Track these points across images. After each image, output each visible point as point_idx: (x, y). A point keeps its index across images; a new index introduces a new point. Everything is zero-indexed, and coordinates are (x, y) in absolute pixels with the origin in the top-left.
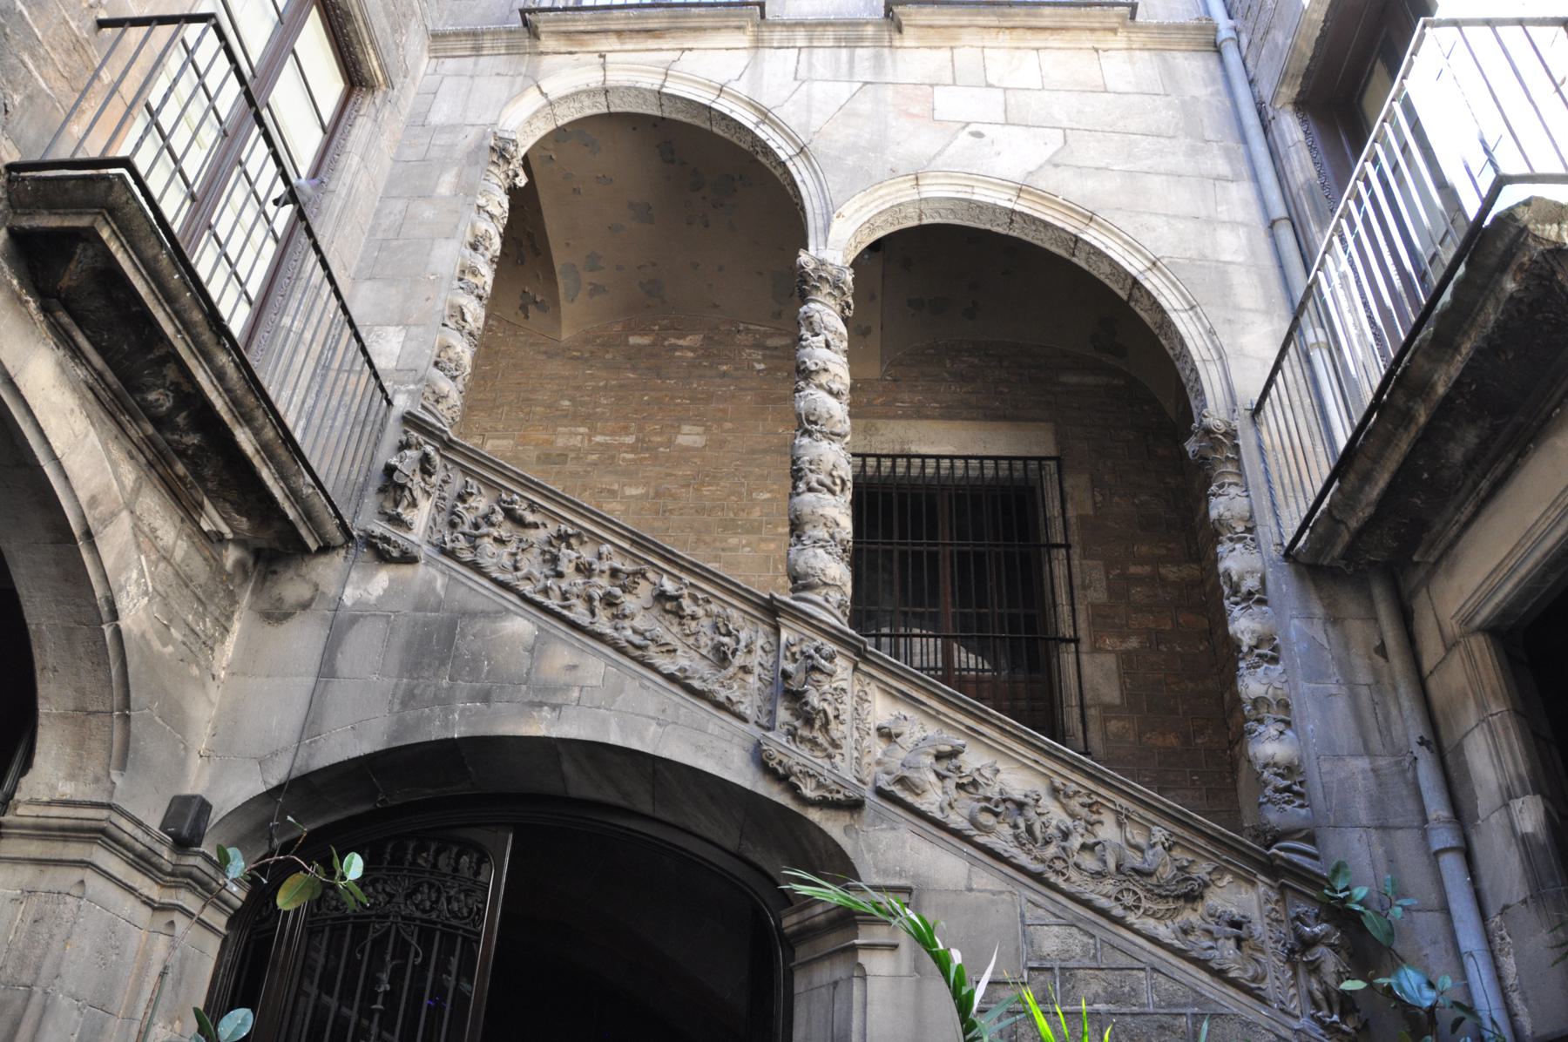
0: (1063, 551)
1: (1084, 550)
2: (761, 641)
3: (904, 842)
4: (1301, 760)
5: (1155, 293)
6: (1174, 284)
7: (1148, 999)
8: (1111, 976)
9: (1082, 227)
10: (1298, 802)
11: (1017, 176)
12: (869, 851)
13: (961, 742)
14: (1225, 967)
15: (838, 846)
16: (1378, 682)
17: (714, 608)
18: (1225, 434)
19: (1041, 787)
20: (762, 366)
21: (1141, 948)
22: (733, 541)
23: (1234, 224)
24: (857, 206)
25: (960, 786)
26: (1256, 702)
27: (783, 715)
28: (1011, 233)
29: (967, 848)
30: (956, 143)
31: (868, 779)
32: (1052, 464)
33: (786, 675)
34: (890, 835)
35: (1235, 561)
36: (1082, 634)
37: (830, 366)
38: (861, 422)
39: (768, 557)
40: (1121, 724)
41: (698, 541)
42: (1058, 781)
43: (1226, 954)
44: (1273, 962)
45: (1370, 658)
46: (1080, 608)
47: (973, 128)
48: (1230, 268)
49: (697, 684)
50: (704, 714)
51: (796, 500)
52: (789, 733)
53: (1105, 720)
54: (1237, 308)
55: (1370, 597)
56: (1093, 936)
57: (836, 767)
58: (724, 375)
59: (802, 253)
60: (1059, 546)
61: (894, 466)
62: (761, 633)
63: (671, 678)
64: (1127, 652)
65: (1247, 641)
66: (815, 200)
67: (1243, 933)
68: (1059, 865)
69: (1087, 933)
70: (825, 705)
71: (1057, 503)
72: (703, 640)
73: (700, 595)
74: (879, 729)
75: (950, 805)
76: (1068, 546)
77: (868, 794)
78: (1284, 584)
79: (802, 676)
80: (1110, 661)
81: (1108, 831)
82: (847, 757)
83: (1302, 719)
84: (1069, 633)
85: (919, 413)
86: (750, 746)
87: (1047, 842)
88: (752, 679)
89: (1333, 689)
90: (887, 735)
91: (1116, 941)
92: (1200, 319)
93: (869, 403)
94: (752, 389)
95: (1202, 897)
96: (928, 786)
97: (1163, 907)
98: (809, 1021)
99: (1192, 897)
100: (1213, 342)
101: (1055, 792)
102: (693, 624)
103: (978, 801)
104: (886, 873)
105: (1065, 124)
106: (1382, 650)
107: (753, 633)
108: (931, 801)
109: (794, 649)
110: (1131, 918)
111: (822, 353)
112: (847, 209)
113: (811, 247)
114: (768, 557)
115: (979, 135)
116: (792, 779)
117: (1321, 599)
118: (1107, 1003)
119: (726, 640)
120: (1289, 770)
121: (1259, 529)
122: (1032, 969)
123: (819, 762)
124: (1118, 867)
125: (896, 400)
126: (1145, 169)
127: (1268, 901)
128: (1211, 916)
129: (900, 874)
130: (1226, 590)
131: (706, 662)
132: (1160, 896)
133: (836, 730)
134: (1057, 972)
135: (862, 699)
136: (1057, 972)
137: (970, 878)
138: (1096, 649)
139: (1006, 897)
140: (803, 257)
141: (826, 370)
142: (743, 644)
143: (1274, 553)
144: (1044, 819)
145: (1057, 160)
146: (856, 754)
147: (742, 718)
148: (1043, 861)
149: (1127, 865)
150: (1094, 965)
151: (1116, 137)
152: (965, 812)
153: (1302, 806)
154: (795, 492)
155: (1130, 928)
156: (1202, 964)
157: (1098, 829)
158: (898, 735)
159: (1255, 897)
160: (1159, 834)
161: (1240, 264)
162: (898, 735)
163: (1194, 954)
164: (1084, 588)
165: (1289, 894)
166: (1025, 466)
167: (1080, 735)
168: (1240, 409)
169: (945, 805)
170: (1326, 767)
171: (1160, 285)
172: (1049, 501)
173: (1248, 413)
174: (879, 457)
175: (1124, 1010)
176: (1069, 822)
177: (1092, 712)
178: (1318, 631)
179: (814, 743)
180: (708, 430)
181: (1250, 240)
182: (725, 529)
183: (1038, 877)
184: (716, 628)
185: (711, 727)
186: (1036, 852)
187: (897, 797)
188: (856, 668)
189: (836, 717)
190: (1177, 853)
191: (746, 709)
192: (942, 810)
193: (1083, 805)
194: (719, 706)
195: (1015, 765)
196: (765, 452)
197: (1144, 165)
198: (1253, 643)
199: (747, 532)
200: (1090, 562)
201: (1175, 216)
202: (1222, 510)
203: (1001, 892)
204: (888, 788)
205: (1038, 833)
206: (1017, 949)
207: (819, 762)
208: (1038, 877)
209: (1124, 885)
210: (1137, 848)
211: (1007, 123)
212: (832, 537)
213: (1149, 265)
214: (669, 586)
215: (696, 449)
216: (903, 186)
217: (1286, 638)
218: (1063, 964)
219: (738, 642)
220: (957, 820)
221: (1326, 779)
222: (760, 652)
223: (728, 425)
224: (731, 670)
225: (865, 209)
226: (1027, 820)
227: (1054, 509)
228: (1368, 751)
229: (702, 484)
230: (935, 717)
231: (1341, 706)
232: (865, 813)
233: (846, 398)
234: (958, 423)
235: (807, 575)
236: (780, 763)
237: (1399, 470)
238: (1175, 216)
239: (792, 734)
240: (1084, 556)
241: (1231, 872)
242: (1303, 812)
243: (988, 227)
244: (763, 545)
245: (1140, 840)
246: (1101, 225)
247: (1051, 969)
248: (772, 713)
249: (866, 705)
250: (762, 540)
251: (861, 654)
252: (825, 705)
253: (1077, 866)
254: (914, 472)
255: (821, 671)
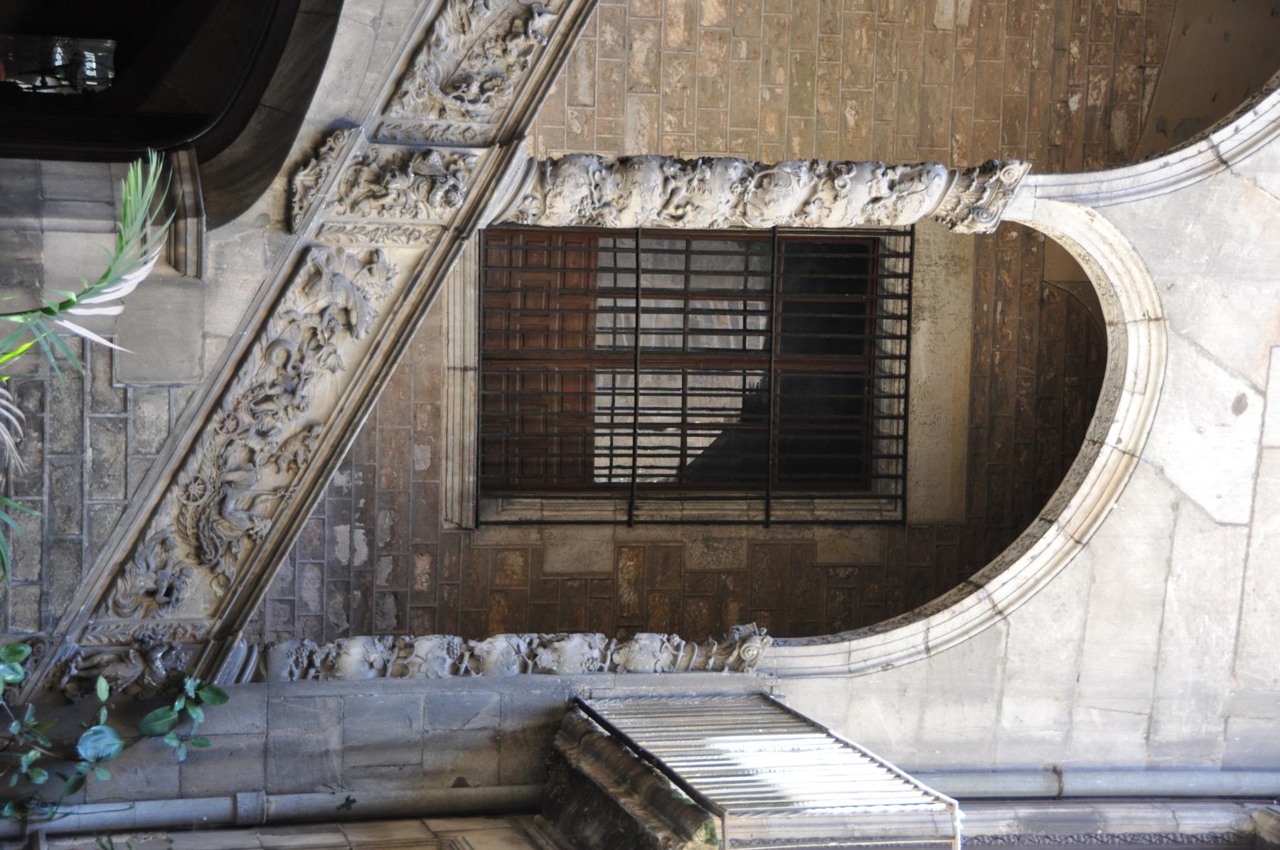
0: (761, 517)
1: (764, 545)
2: (476, 126)
3: (252, 273)
4: (339, 678)
5: (956, 608)
6: (966, 632)
7: (97, 500)
8: (119, 467)
9: (1070, 530)
10: (297, 672)
11: (1158, 451)
12: (243, 238)
13: (363, 335)
14: (127, 576)
15: (247, 207)
16: (425, 774)
17: (517, 75)
18: (740, 660)
19: (314, 412)
20: (1074, 103)
21: (146, 499)
22: (780, 76)
23: (1069, 726)
24: (1111, 238)
25: (314, 332)
26: (410, 647)
27: (388, 152)
28: (1085, 442)
29: (247, 336)
30: (1223, 377)
31: (322, 239)
32: (898, 515)
33: (426, 154)
34: (259, 259)
35: (578, 650)
36: (641, 533)
37: (841, 203)
38: (969, 253)
39: (754, 124)
40: (518, 569)
41: (781, 27)
42: (320, 430)
43: (141, 579)
44: (134, 624)
45: (453, 771)
46: (678, 532)
47: (1254, 400)
48: (990, 709)
49: (422, 58)
50: (387, 68)
51: (655, 164)
52: (365, 158)
53: (523, 550)
54: (924, 705)
55: (525, 784)
56: (158, 452)
57: (328, 206)
58: (1061, 49)
59: (1027, 166)
60: (767, 511)
61: (895, 296)
62: (487, 126)
63: (430, 29)
64: (615, 587)
65: (480, 647)
66: (1128, 182)
67: (161, 597)
68: (230, 424)
69: (161, 446)
70: (393, 196)
71: (834, 516)
72: (478, 64)
73: (530, 58)
74: (377, 251)
75: (293, 321)
76: (766, 523)
77: (307, 236)
78: (541, 694)
79: (426, 171)
80: (603, 563)
81: (268, 478)
82: (342, 218)
83: (384, 686)
84: (642, 515)
85: (982, 333)
86: (353, 117)
87: (254, 415)
88: (433, 117)
89: (419, 725)
90: (371, 260)
91: (153, 474)
92: (910, 656)
93: (1001, 265)
94: (1031, 93)
95: (201, 563)
96: (312, 299)
97: (189, 523)
98: (81, 177)
99: (199, 554)
100: (874, 666)
101: (309, 427)
102: (499, 52)
103: (300, 349)
104: (220, 254)
105: (1259, 528)
106: (460, 783)
107: (486, 116)
108: (298, 302)
109: (461, 163)
110: (177, 491)
111: (861, 194)
112: (1102, 224)
113: (1041, 179)
114: (754, 124)
115: (1240, 406)
116: (314, 162)
117: (524, 731)
118: (93, 461)
119: (475, 88)
120: (330, 667)
121: (611, 676)
122: (125, 391)
123: (334, 187)
124: (230, 483)
125: (1007, 302)
126: (1169, 625)
127: (195, 627)
128: (181, 571)
129: (219, 268)
130: (546, 637)
131: (452, 66)
132: (199, 521)
133: (369, 206)
134: (123, 415)
135: (410, 235)
136: (123, 415)
137: (216, 336)
138: (619, 547)
139: (197, 371)
140: (1017, 170)
141: (836, 198)
142: (471, 107)
143: (582, 689)
144: (281, 414)
145: (1186, 509)
146: (349, 227)
147: (386, 108)
148: (236, 409)
149: (230, 491)
150: (130, 451)
151: (1234, 594)
152: (287, 336)
153: (291, 674)
154: (663, 161)
155: (168, 489)
156: (131, 555)
157: (272, 468)
158: (370, 270)
159: (200, 616)
160: (263, 527)
161: (998, 721)
162: (370, 270)
163: (140, 548)
164: (707, 541)
165: (200, 647)
166: (895, 477)
167: (504, 518)
168: (771, 682)
169: (293, 316)
170: (332, 703)
171: (967, 616)
172: (838, 503)
173: (767, 690)
174: (909, 276)
175: (86, 476)
176: (280, 439)
177: (533, 535)
178: (486, 719)
179: (353, 184)
180: (962, 30)
181: (1041, 741)
182: (800, 64)
183: (218, 403)
184: (492, 77)
185: (372, 77)
186: (244, 403)
187: (301, 267)
188: (445, 228)
189: (383, 207)
190: (246, 543)
191: (396, 112)
192: (287, 312)
193: (296, 455)
194: (399, 82)
195: (340, 389)
196: (924, 117)
197: (1175, 620)
198: (477, 652)
199: (794, 95)
200: (744, 550)
201: (1080, 651)
202: (642, 642)
203: (202, 366)
204: (309, 258)
205: (265, 406)
206: (145, 379)
207: (334, 187)
208: (218, 403)
209: (210, 487)
210: (252, 505)
211: (1261, 448)
212: (607, 204)
213: (1000, 607)
214: (541, 23)
215: (930, 16)
216: (1146, 300)
217: (476, 684)
218: (130, 422)
219: (473, 102)
220: (277, 327)
221: (319, 701)
222: (464, 126)
223: (970, 60)
224: (438, 95)
225: (1106, 249)
226: (278, 396)
227: (825, 509)
228: (347, 750)
229: (872, 27)
230: (392, 310)
231: (398, 730)
232: (282, 234)
233: (797, 223)
234: (964, 387)
235: (555, 175)
236: (331, 149)
237: (593, 784)
238: (1080, 651)
239: (364, 162)
240: (753, 546)
241: (226, 595)
242: (285, 673)
243: (1097, 413)
244: (772, 117)
245: (259, 509)
246: (1068, 553)
247: (125, 410)
248: (392, 140)
249: (404, 238)
250: (781, 115)
251: (461, 233)
252: (393, 196)
253: (231, 443)
254: (888, 325)
255: (430, 191)
